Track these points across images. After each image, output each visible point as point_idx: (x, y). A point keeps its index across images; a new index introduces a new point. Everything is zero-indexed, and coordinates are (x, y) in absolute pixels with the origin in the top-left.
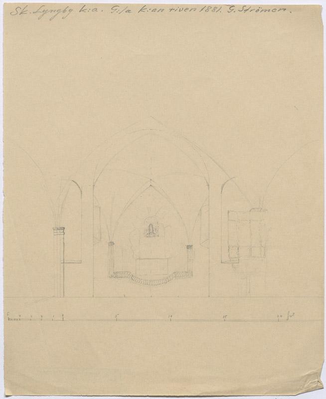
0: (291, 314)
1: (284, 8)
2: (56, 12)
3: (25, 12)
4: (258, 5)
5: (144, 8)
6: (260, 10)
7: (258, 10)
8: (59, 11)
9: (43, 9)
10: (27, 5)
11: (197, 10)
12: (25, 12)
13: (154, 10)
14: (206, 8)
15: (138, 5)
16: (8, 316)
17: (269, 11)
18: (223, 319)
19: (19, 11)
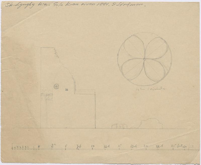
0: (79, 146)
1: (94, 3)
2: (26, 6)
3: (69, 4)
4: (129, 2)
5: (69, 3)
6: (130, 4)
7: (129, 4)
8: (28, 5)
9: (20, 4)
10: (12, 2)
11: (95, 5)
12: (69, 4)
13: (74, 4)
14: (100, 4)
15: (38, 2)
16: (66, 148)
17: (135, 5)
18: (38, 148)
19: (9, 5)
